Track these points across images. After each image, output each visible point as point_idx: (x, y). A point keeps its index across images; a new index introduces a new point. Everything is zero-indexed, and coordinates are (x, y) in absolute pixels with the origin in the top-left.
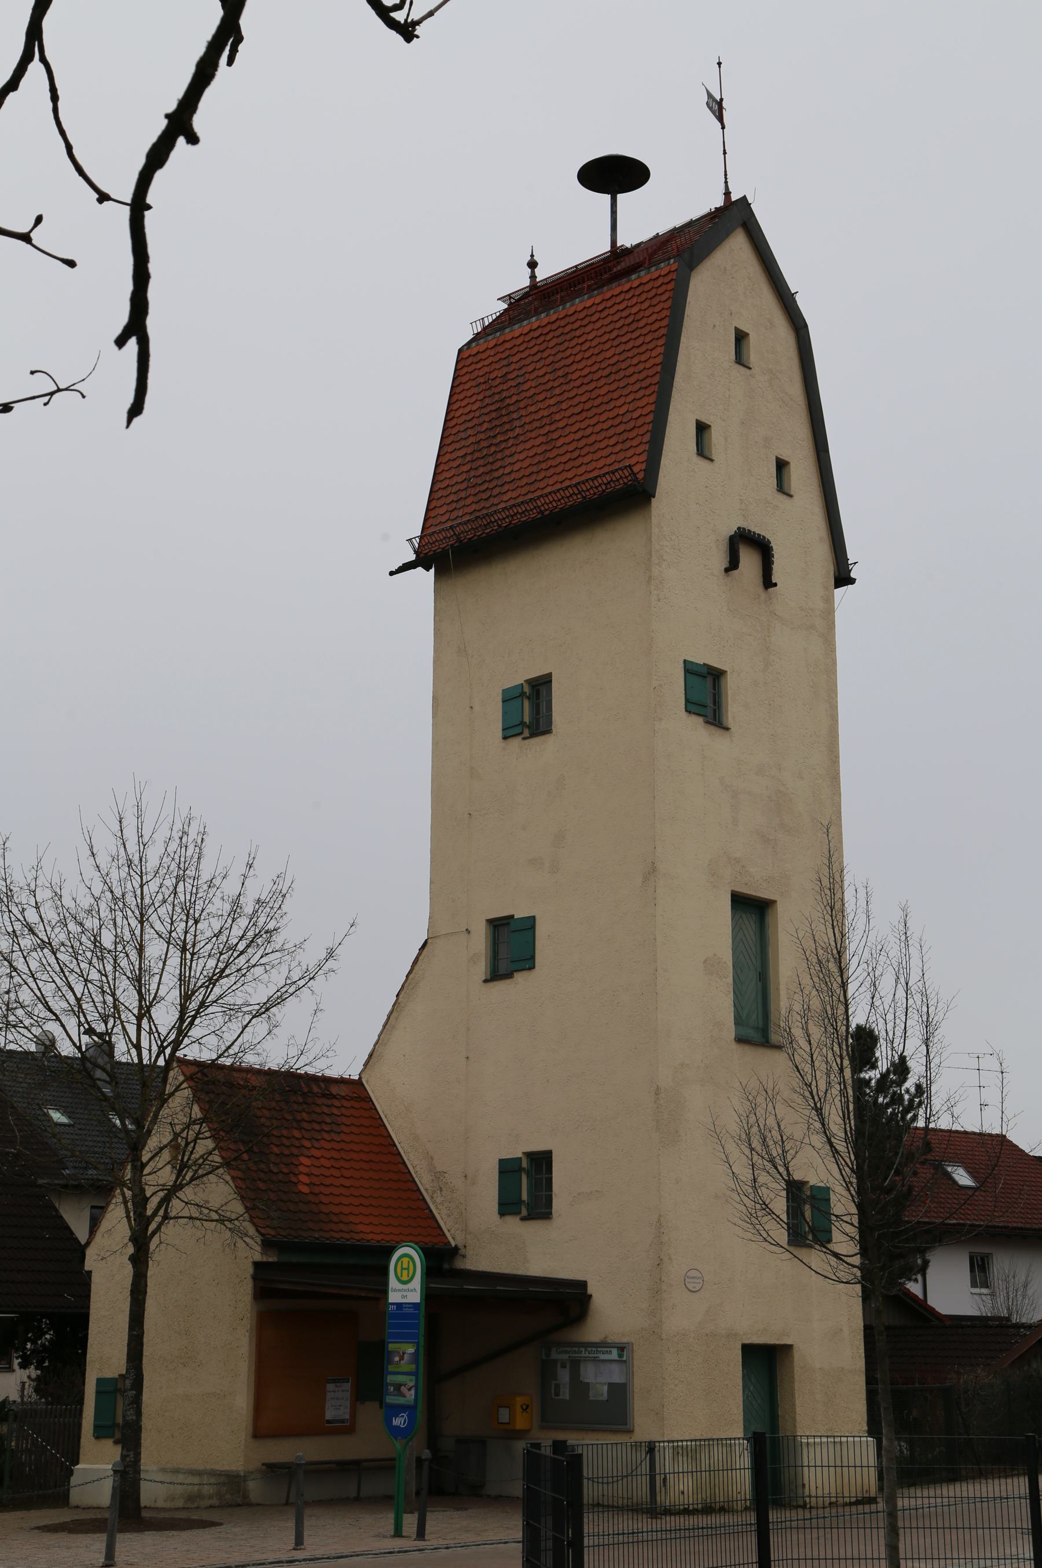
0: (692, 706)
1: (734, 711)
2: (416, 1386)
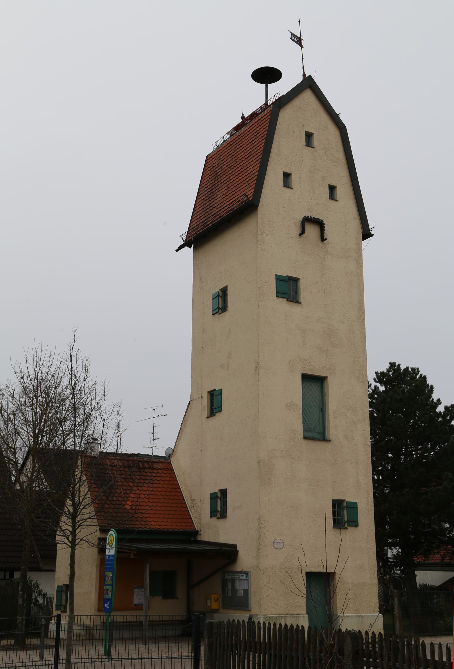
0: (280, 294)
1: (303, 295)
2: (112, 590)
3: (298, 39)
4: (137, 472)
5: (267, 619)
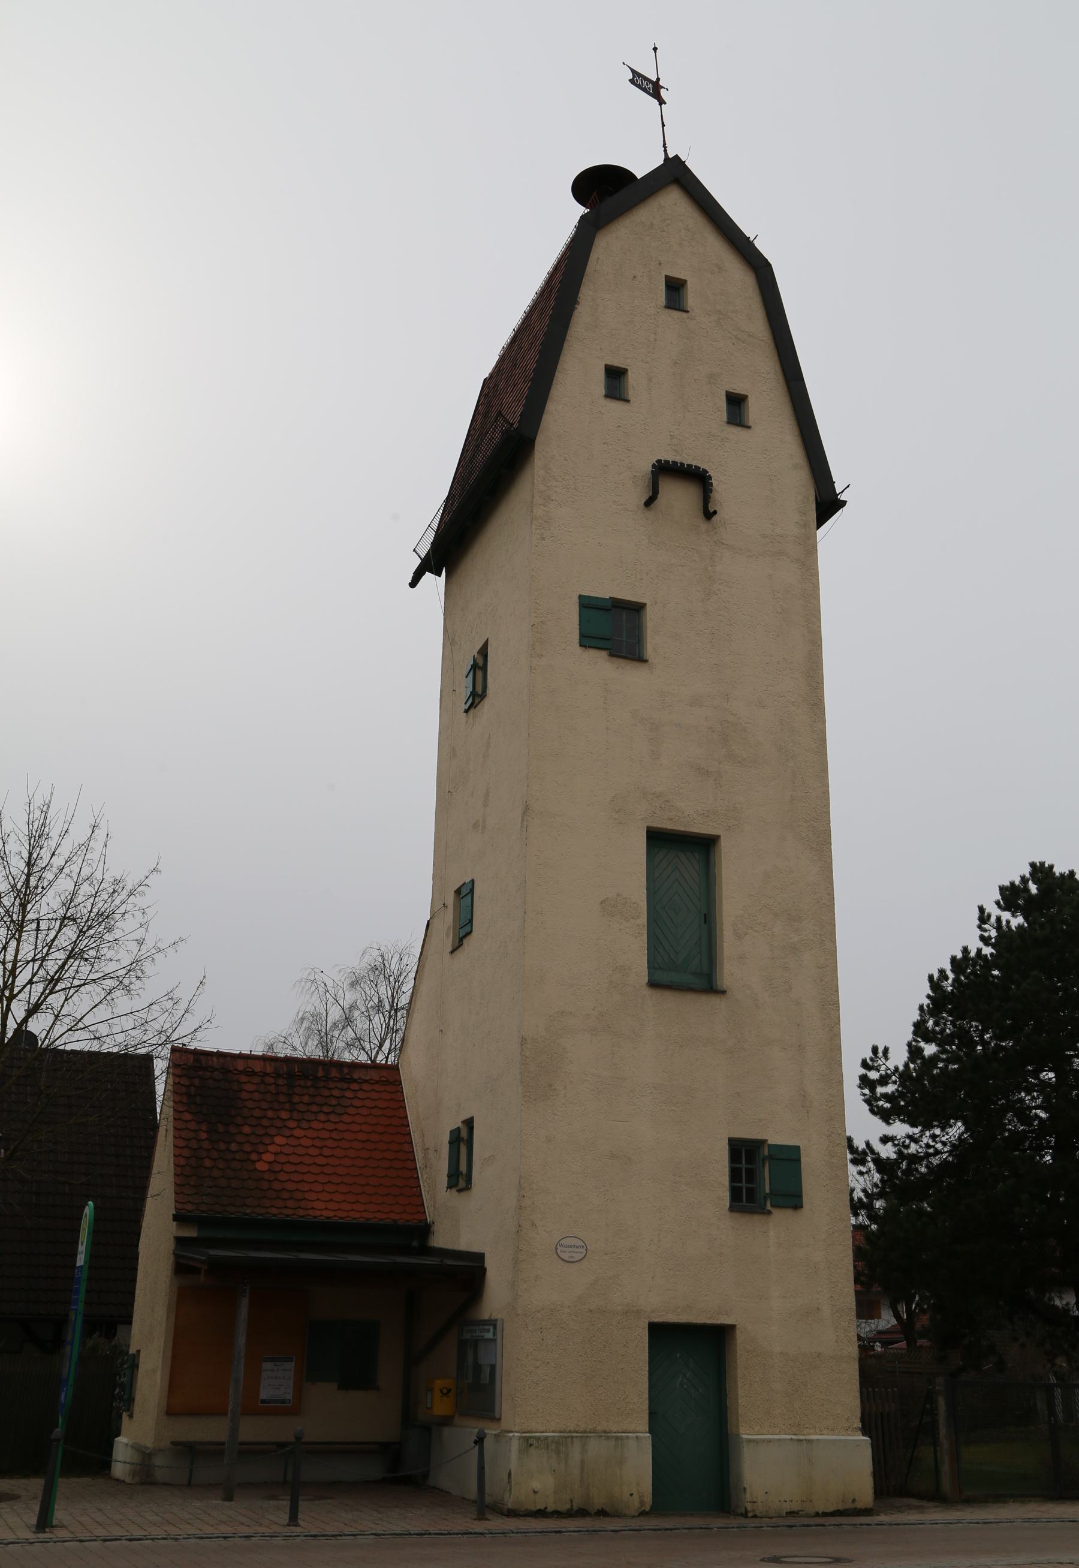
0: (588, 640)
1: (654, 642)
3: (650, 86)
4: (308, 1087)
5: (531, 1441)
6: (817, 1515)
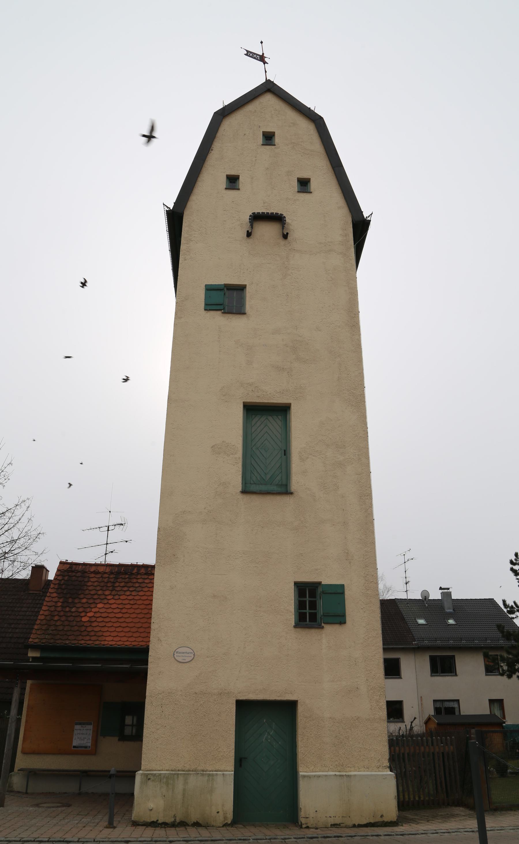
5: (149, 777)
6: (354, 826)
